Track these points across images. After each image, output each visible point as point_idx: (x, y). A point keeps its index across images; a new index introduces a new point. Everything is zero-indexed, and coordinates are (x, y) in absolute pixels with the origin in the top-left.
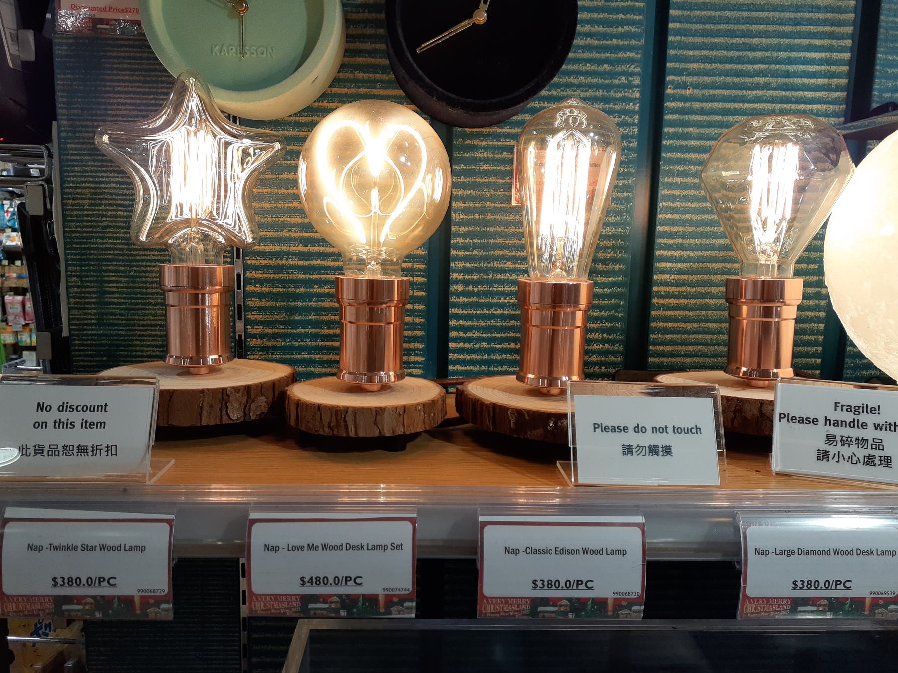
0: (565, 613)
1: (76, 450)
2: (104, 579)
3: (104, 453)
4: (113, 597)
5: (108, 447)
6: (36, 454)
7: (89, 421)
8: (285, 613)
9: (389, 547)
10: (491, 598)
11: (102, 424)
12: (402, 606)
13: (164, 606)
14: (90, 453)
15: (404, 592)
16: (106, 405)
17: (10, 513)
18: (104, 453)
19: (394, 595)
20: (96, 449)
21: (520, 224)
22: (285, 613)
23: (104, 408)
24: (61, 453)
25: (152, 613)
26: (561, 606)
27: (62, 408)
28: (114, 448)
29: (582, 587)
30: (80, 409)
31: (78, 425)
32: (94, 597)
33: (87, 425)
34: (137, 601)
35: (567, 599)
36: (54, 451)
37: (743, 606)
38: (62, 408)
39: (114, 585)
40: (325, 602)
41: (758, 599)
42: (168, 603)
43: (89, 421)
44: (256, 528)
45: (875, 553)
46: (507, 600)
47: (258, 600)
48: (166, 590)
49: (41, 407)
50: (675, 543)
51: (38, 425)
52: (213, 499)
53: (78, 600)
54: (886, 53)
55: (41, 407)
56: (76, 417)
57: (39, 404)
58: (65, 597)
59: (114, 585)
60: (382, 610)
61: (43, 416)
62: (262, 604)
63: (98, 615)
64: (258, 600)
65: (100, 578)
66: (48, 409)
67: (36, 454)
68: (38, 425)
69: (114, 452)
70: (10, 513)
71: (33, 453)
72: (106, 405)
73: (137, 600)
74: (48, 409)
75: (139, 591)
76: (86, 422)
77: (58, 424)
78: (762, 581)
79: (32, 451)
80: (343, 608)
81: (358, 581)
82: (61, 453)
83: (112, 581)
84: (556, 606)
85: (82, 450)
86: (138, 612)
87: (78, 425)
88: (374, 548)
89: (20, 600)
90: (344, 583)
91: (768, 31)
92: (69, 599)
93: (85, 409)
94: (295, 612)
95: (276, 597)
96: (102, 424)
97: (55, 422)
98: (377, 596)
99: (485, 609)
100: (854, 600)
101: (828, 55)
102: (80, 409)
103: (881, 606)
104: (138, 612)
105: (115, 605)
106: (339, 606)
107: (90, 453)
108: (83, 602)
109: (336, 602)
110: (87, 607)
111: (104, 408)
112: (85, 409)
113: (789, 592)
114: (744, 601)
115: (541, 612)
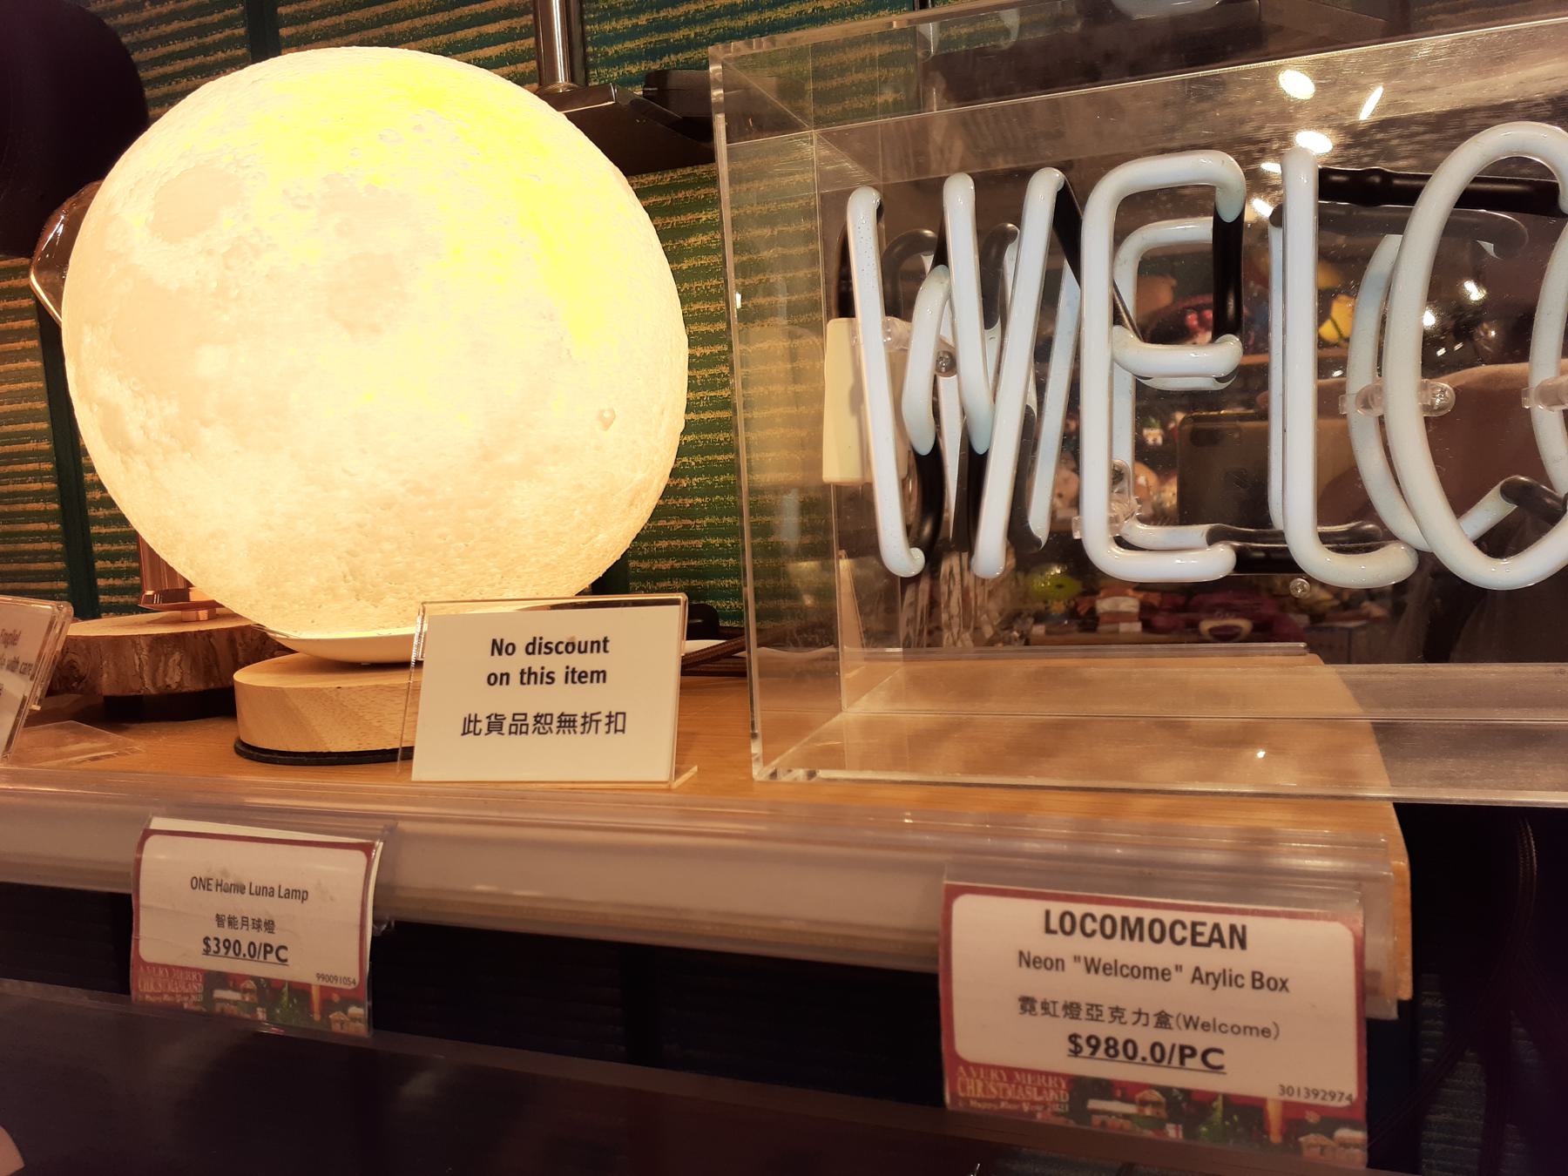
1: (555, 724)
3: (602, 727)
4: (1213, 1096)
5: (609, 716)
6: (490, 731)
7: (579, 670)
8: (1032, 1114)
11: (600, 675)
12: (1331, 1136)
13: (1344, 1133)
14: (579, 729)
15: (1335, 1103)
16: (606, 641)
17: (157, 823)
18: (602, 727)
19: (334, 989)
20: (590, 720)
22: (1032, 1114)
23: (601, 645)
24: (531, 728)
27: (533, 647)
28: (620, 717)
29: (272, 957)
30: (562, 648)
31: (559, 676)
32: (1165, 1091)
33: (576, 677)
34: (1273, 1112)
36: (519, 725)
38: (533, 647)
39: (1217, 1069)
40: (1126, 1099)
43: (579, 670)
44: (152, 841)
47: (969, 1075)
48: (1355, 1096)
49: (498, 647)
50: (489, 894)
51: (495, 679)
52: (1029, 846)
53: (1125, 1091)
54: (600, 20)
55: (498, 647)
56: (556, 664)
57: (494, 642)
59: (1217, 1069)
61: (501, 664)
62: (980, 1085)
63: (1172, 1132)
65: (1182, 1048)
66: (510, 649)
67: (490, 731)
68: (495, 679)
69: (620, 727)
70: (157, 823)
71: (485, 730)
72: (606, 641)
73: (315, 994)
74: (510, 649)
75: (319, 976)
76: (574, 671)
77: (528, 676)
78: (166, 940)
79: (483, 726)
80: (1173, 1119)
81: (1212, 1058)
82: (531, 728)
83: (1212, 1058)
85: (567, 722)
86: (317, 1017)
87: (559, 676)
88: (289, 894)
89: (994, 1075)
90: (1176, 1060)
91: (415, 29)
92: (1105, 1088)
93: (571, 647)
94: (195, 1003)
95: (1010, 1073)
96: (600, 675)
97: (522, 673)
99: (964, 1087)
101: (508, 46)
102: (562, 648)
104: (317, 1017)
107: (579, 729)
108: (1139, 1096)
109: (1155, 1104)
110: (1148, 1111)
111: (601, 645)
112: (571, 647)
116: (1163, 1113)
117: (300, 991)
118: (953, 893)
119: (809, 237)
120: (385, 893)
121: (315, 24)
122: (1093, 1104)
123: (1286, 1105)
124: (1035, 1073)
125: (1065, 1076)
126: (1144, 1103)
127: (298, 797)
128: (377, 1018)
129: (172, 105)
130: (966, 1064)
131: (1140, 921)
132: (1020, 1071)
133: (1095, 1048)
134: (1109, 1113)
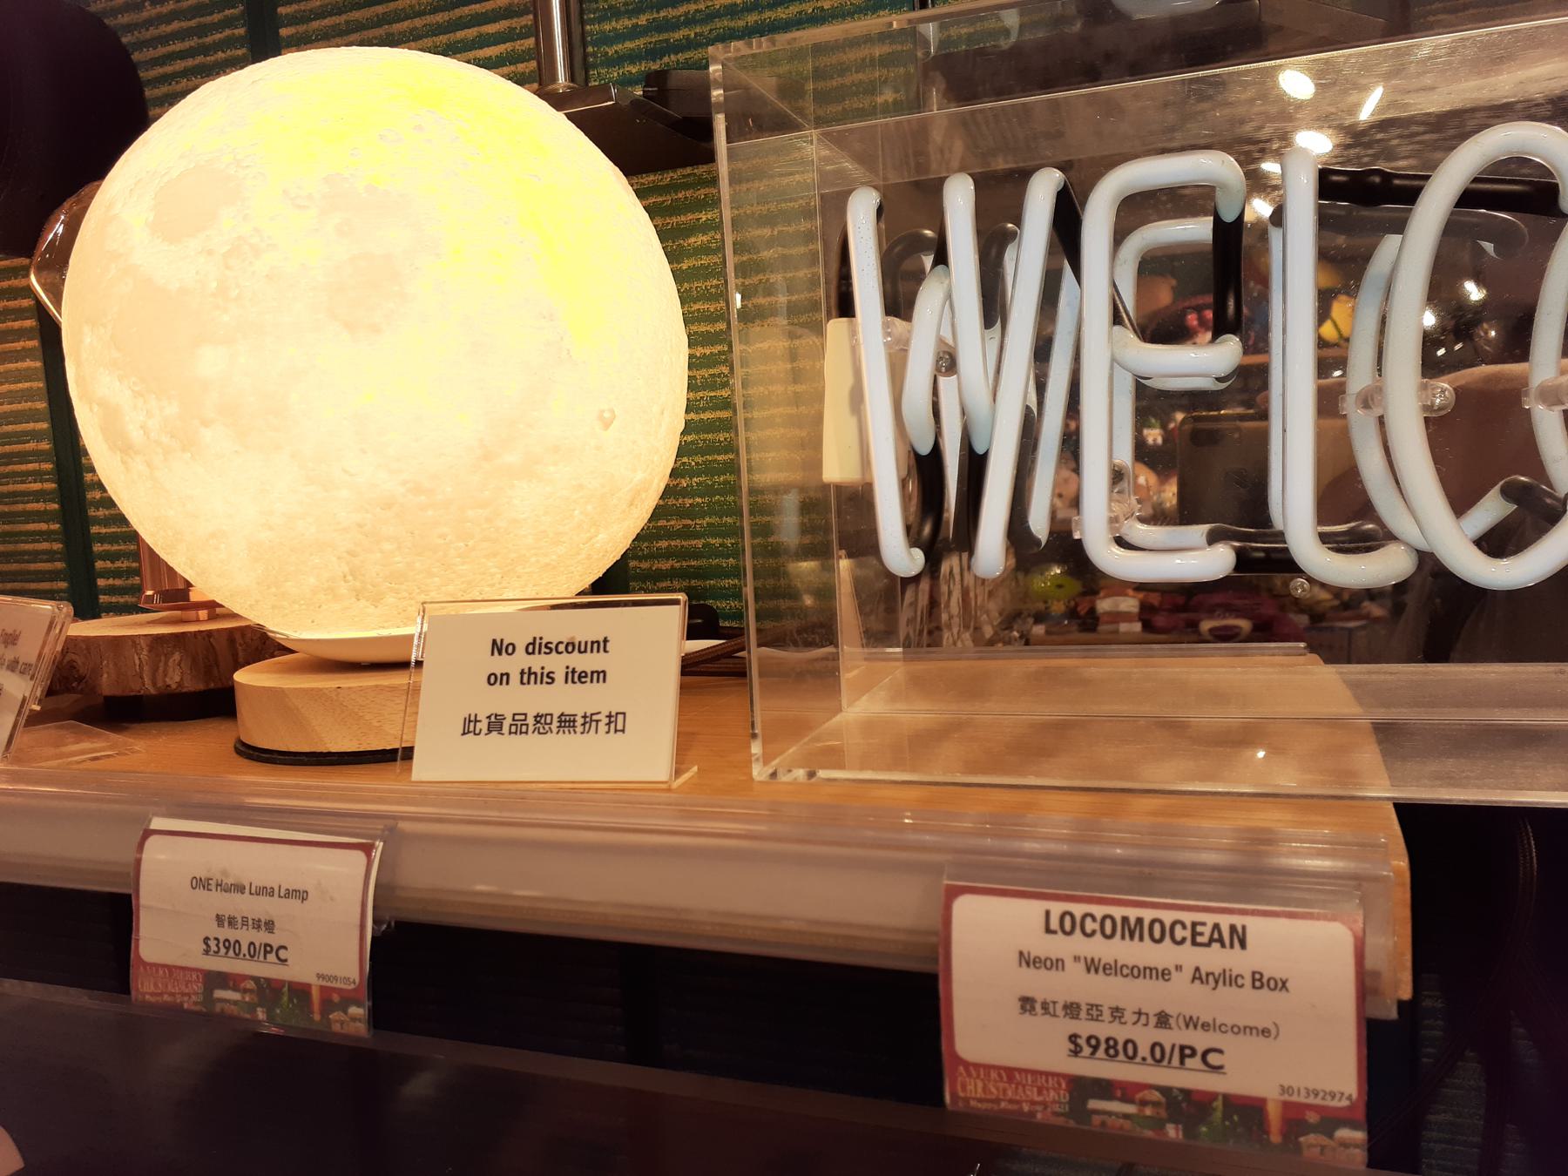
0: (1158, 1124)
1: (555, 724)
3: (602, 727)
4: (1213, 1096)
5: (609, 716)
6: (490, 731)
7: (579, 670)
8: (1032, 1114)
11: (600, 675)
12: (1331, 1136)
13: (1344, 1133)
14: (579, 729)
15: (1335, 1103)
16: (606, 641)
17: (157, 823)
18: (602, 727)
19: (334, 989)
20: (590, 720)
22: (1032, 1114)
23: (601, 645)
24: (531, 728)
27: (533, 647)
28: (620, 717)
29: (272, 957)
30: (562, 648)
31: (559, 676)
32: (1165, 1091)
33: (576, 677)
34: (1273, 1112)
36: (519, 725)
38: (533, 647)
39: (1217, 1069)
40: (1126, 1099)
43: (579, 670)
44: (152, 841)
47: (969, 1075)
48: (1355, 1096)
49: (498, 647)
50: (489, 894)
51: (495, 679)
53: (1125, 1091)
54: (600, 20)
55: (498, 647)
56: (556, 664)
57: (494, 642)
59: (1217, 1069)
61: (501, 664)
62: (980, 1085)
63: (1172, 1132)
65: (1182, 1048)
66: (510, 649)
67: (490, 731)
68: (495, 679)
69: (620, 727)
70: (157, 823)
71: (485, 730)
72: (606, 641)
73: (315, 994)
74: (510, 649)
75: (319, 976)
76: (574, 671)
77: (528, 676)
78: (166, 940)
79: (483, 726)
80: (1173, 1119)
81: (1212, 1058)
82: (531, 728)
83: (1212, 1058)
85: (567, 722)
86: (317, 1017)
87: (559, 676)
88: (289, 894)
89: (994, 1075)
90: (1176, 1060)
92: (1105, 1088)
93: (571, 647)
94: (195, 1003)
95: (1010, 1073)
96: (600, 675)
97: (522, 673)
99: (964, 1087)
101: (508, 46)
102: (562, 648)
104: (317, 1017)
107: (579, 729)
108: (1139, 1096)
109: (1155, 1104)
110: (1148, 1111)
111: (601, 645)
112: (571, 647)
116: (1163, 1113)
117: (300, 991)
118: (953, 893)
119: (809, 237)
120: (385, 893)
122: (1093, 1104)
123: (1286, 1105)
124: (1035, 1073)
125: (1065, 1076)
126: (1144, 1103)
127: (298, 797)
128: (377, 1018)
129: (172, 105)
130: (966, 1064)
131: (1140, 921)
132: (1020, 1071)
133: (1095, 1048)
134: (1109, 1113)
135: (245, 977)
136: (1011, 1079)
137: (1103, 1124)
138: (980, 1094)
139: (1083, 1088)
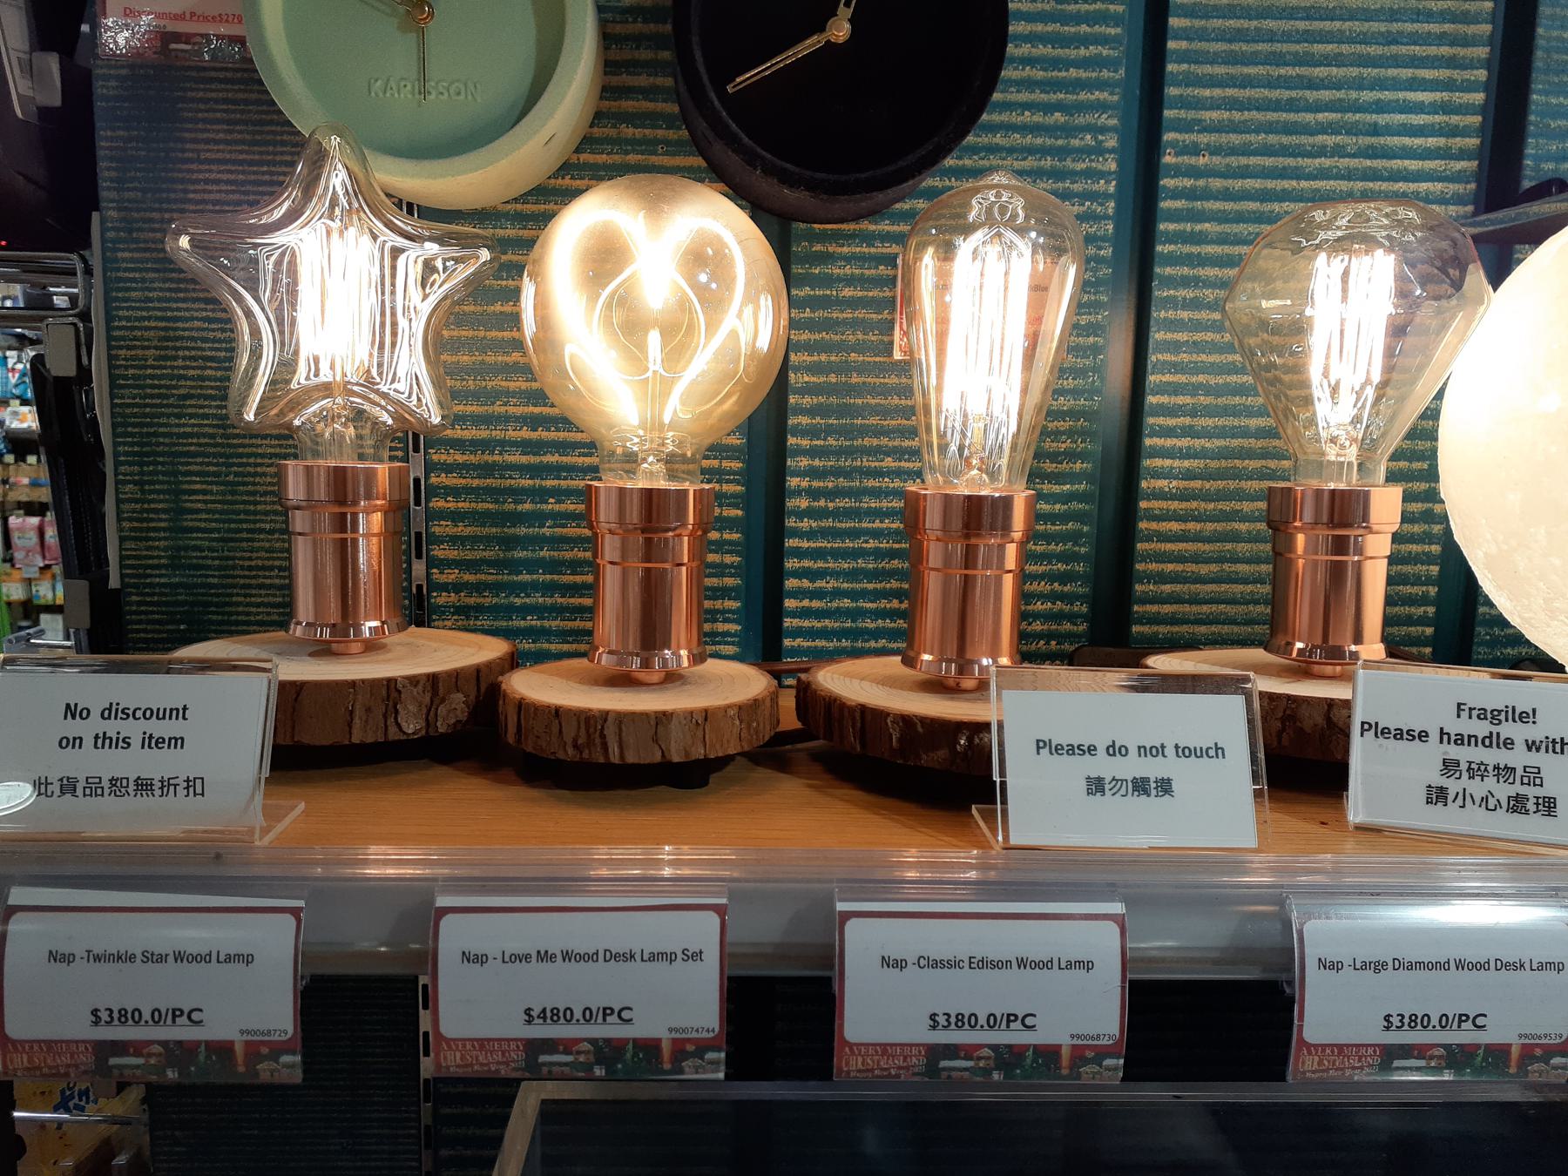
0: (987, 1072)
1: (132, 787)
2: (182, 1011)
3: (181, 791)
4: (198, 1043)
5: (188, 781)
6: (63, 793)
7: (156, 736)
8: (497, 1071)
9: (680, 955)
10: (858, 1045)
11: (178, 742)
12: (702, 1058)
13: (286, 1059)
14: (158, 792)
15: (705, 1035)
16: (185, 708)
17: (17, 896)
18: (181, 791)
19: (689, 1040)
20: (167, 785)
21: (907, 391)
22: (497, 1071)
23: (181, 713)
24: (107, 791)
25: (266, 1071)
26: (980, 1058)
27: (108, 713)
28: (199, 782)
29: (1017, 1025)
30: (139, 714)
31: (136, 742)
32: (164, 1044)
33: (151, 742)
34: (239, 1049)
35: (990, 1046)
36: (94, 788)
37: (1297, 1059)
38: (108, 713)
39: (199, 1023)
40: (567, 1052)
41: (1324, 1046)
42: (294, 1053)
43: (156, 736)
44: (447, 923)
45: (1527, 966)
46: (885, 1049)
47: (450, 1048)
48: (291, 1031)
49: (71, 711)
50: (1178, 949)
51: (66, 743)
52: (371, 871)
53: (135, 1048)
54: (1546, 93)
55: (71, 711)
56: (133, 729)
57: (68, 706)
58: (114, 1043)
59: (199, 1023)
60: (667, 1066)
61: (74, 728)
62: (458, 1055)
63: (172, 1074)
64: (450, 1048)
65: (174, 1011)
66: (84, 714)
67: (63, 793)
68: (66, 743)
69: (199, 790)
70: (17, 896)
71: (57, 792)
72: (185, 708)
73: (239, 1049)
74: (84, 714)
75: (242, 1032)
76: (151, 737)
77: (102, 740)
78: (1331, 1015)
79: (56, 788)
80: (598, 1062)
81: (625, 1015)
82: (107, 791)
83: (195, 1016)
84: (971, 1059)
85: (144, 786)
86: (241, 1069)
87: (136, 742)
88: (654, 957)
89: (36, 1048)
90: (600, 1019)
91: (1341, 54)
92: (120, 1047)
93: (149, 714)
94: (515, 1069)
95: (482, 1043)
96: (178, 742)
97: (97, 737)
98: (659, 1041)
99: (847, 1064)
100: (1491, 1049)
101: (1445, 95)
102: (139, 714)
103: (1538, 1060)
104: (241, 1069)
105: (202, 1058)
106: (592, 1058)
107: (158, 792)
108: (145, 1051)
109: (587, 1052)
110: (152, 1061)
111: (181, 713)
112: (149, 714)
113: (1377, 1035)
114: (1299, 1050)
115: (944, 1069)
121: (1217, 23)
135: (980, 1046)
136: (884, 1052)
137: (949, 1077)
138: (860, 1066)
139: (936, 1053)
